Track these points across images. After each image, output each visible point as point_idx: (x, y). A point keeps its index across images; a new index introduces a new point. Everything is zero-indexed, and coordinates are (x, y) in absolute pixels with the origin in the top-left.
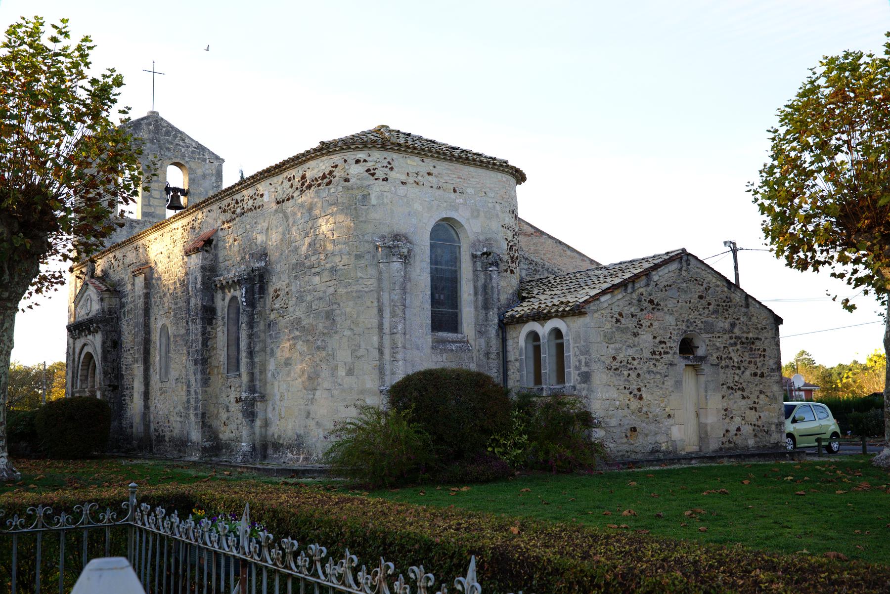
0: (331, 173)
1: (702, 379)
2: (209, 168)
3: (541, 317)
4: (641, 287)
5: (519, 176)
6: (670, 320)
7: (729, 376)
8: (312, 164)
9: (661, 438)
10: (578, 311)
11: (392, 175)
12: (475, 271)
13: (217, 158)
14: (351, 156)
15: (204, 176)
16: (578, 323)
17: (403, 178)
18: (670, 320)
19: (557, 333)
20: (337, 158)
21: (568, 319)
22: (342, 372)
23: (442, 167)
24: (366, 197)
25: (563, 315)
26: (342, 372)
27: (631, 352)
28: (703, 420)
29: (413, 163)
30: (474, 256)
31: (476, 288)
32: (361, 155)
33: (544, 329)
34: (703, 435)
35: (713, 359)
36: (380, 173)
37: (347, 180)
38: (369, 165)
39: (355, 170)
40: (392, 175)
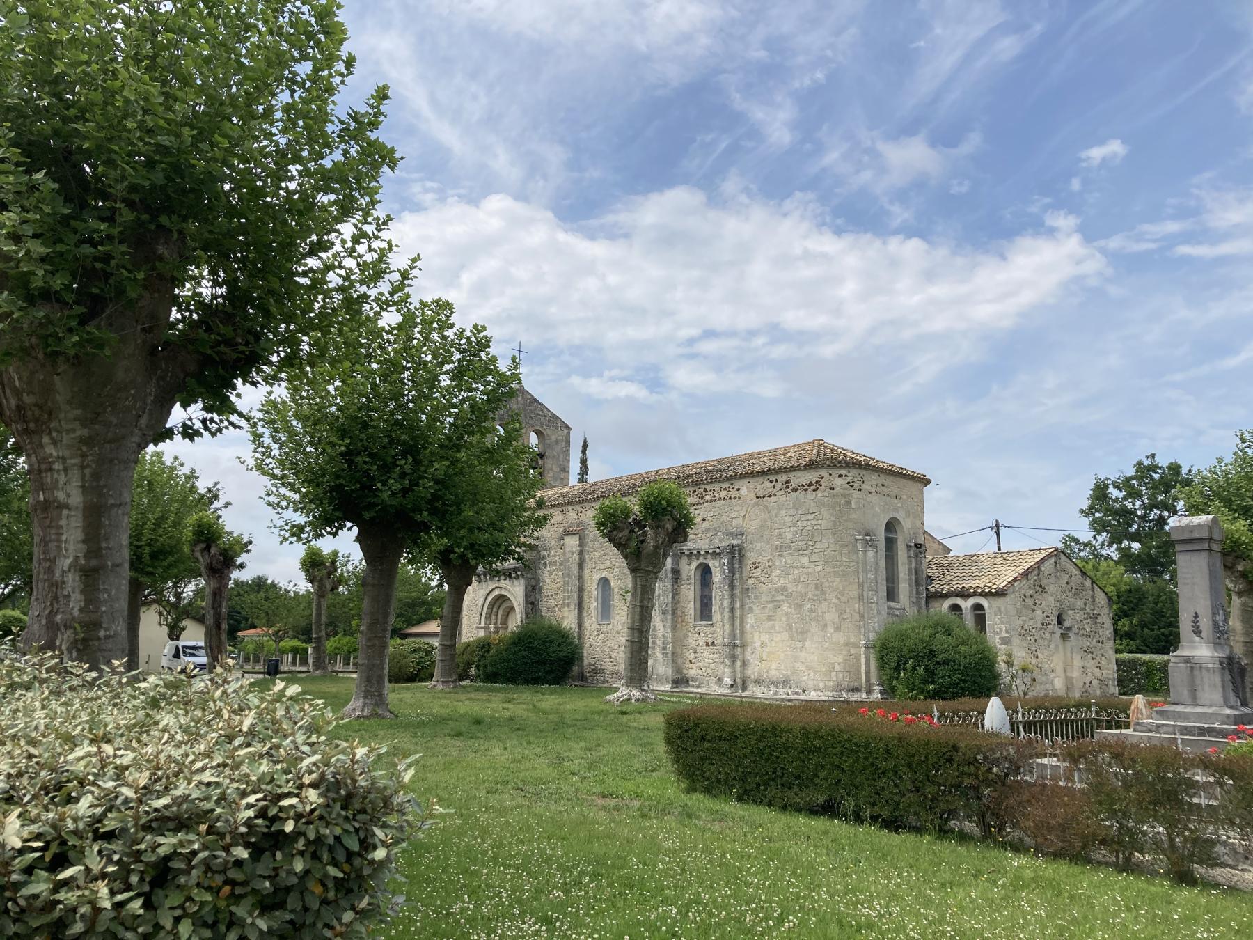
0: (817, 482)
1: (1069, 644)
2: (561, 435)
3: (964, 594)
4: (1033, 577)
5: (926, 482)
6: (1051, 599)
7: (1084, 642)
8: (798, 474)
9: (1049, 687)
10: (1001, 593)
11: (864, 486)
12: (909, 557)
13: (567, 426)
14: (835, 472)
15: (557, 442)
16: (998, 602)
17: (869, 488)
18: (1051, 599)
19: (978, 607)
20: (824, 473)
21: (990, 598)
22: (830, 629)
23: (889, 480)
24: (848, 503)
25: (984, 595)
26: (830, 629)
27: (1031, 623)
28: (1069, 675)
29: (874, 478)
30: (909, 547)
31: (910, 570)
32: (843, 472)
33: (966, 605)
34: (1069, 685)
35: (1075, 630)
36: (856, 485)
37: (832, 489)
38: (849, 479)
39: (839, 482)
40: (864, 486)
